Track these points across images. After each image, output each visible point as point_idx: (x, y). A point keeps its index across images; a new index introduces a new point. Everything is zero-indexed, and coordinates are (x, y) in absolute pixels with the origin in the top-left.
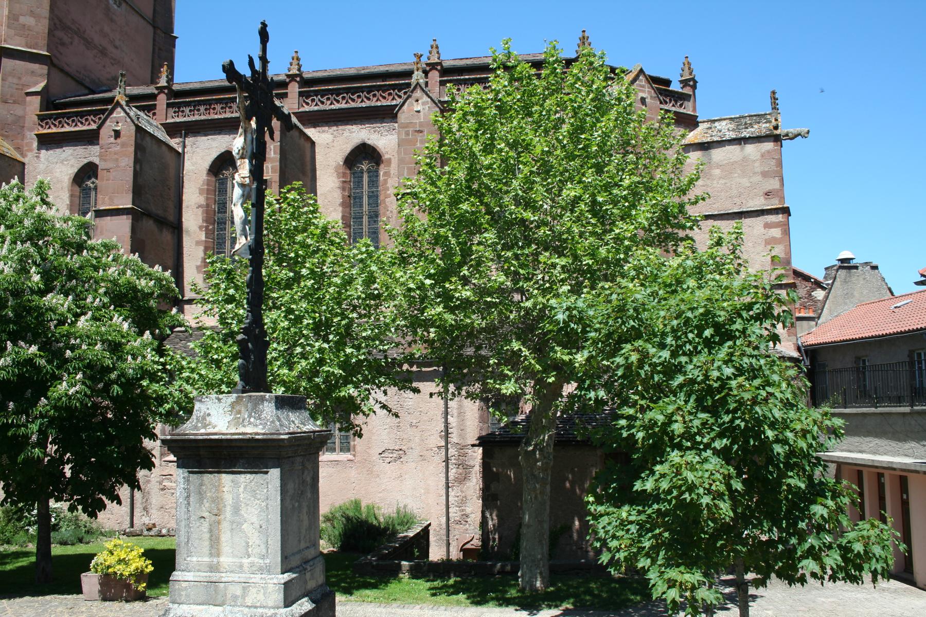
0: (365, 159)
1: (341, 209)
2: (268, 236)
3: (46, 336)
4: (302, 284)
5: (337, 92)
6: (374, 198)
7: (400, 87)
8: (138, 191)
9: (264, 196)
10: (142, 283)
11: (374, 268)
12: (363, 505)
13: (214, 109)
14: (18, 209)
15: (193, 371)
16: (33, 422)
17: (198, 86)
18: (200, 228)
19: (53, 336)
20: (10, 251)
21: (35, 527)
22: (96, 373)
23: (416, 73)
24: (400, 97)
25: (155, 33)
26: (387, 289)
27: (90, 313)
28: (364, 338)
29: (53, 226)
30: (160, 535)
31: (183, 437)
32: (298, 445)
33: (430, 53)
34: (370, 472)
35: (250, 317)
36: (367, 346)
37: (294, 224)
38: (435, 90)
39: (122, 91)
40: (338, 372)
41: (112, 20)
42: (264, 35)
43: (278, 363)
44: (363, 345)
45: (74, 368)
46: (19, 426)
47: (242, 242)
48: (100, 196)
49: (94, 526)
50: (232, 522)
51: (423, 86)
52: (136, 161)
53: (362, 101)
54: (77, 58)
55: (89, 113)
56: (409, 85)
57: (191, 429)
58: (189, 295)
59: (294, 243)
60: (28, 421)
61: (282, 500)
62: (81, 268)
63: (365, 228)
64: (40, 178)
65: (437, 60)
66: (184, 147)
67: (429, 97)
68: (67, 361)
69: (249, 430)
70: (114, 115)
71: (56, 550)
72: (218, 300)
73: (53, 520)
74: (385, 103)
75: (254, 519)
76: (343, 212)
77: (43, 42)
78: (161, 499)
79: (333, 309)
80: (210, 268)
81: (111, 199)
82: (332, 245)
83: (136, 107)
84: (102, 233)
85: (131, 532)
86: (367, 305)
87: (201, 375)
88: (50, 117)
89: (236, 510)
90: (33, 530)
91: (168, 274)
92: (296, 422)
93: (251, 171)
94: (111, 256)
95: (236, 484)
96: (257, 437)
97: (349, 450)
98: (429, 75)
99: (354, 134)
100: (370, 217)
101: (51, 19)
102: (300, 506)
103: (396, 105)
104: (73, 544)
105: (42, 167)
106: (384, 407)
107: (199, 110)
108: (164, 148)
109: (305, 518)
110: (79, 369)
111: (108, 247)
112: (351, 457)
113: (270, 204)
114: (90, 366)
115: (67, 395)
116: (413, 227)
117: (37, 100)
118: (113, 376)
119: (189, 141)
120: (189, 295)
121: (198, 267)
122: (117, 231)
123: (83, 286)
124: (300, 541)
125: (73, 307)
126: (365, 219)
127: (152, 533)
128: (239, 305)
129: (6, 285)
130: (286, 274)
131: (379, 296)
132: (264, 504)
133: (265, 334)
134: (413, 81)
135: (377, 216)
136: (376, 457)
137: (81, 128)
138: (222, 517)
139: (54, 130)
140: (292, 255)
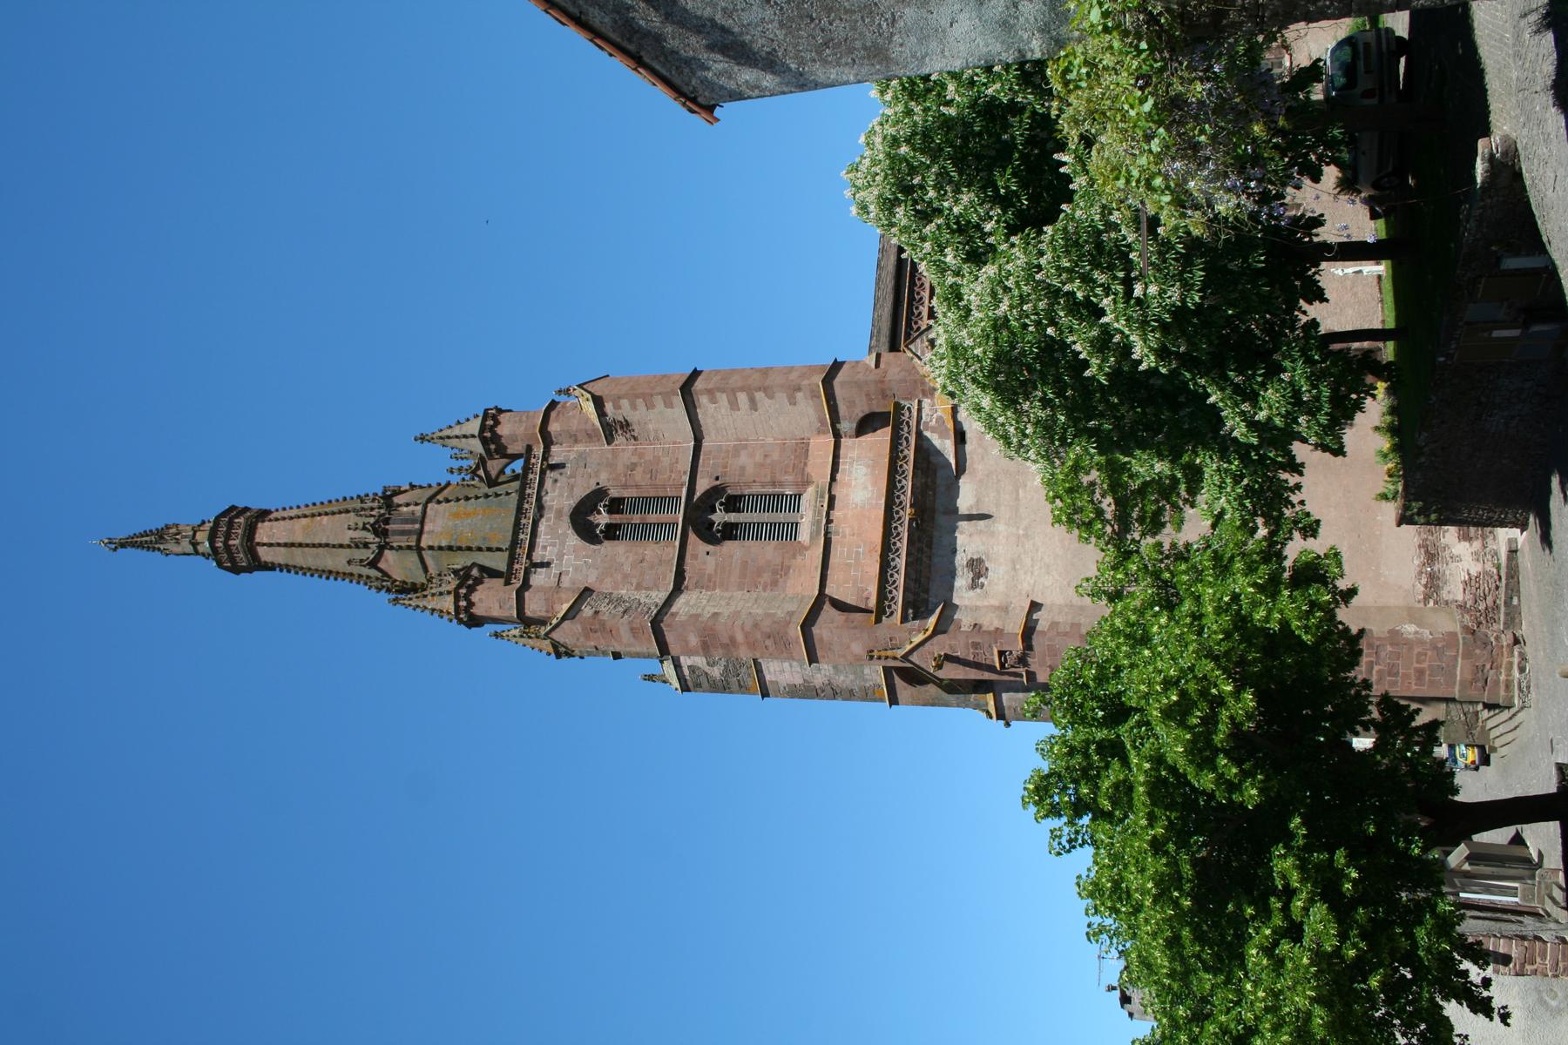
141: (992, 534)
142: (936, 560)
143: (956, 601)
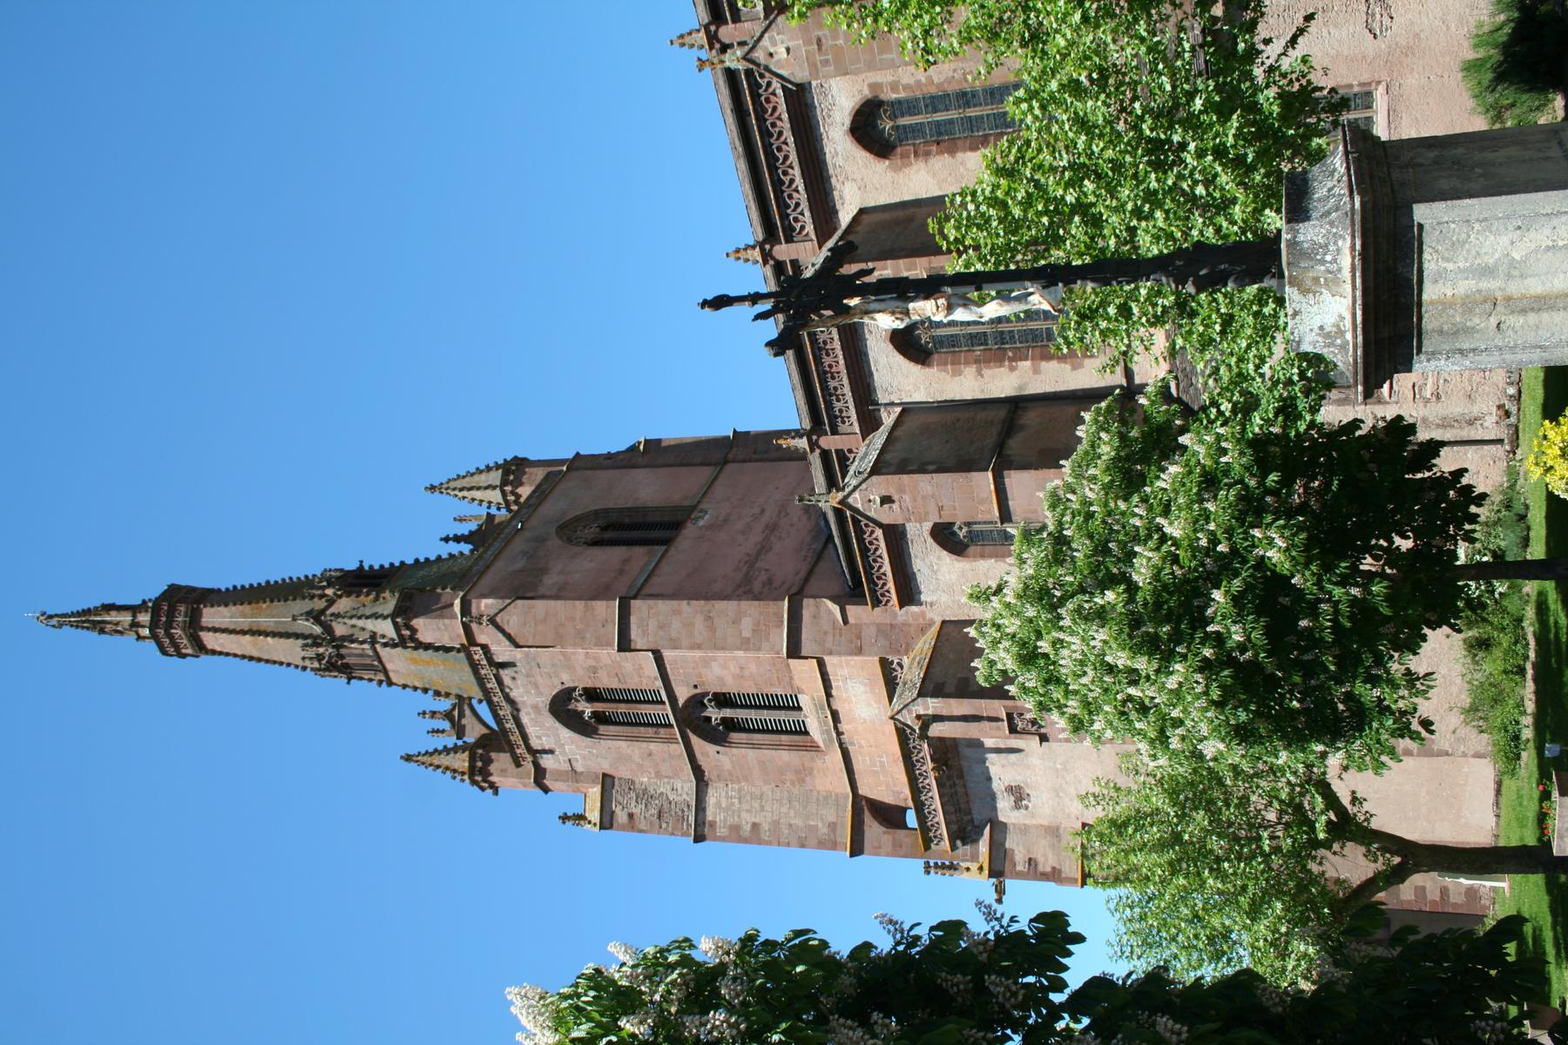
0: (875, 126)
1: (960, 155)
2: (1022, 259)
3: (1196, 579)
4: (1092, 199)
5: (778, 184)
6: (936, 102)
7: (754, 86)
8: (966, 465)
9: (958, 275)
10: (1106, 451)
11: (1054, 85)
12: (1471, 55)
13: (830, 366)
14: (1012, 625)
15: (1241, 360)
16: (1330, 593)
17: (800, 393)
18: (1012, 369)
19: (1196, 570)
20: (1073, 633)
21: (1496, 583)
22: (1250, 509)
23: (728, 64)
24: (769, 84)
25: (733, 461)
26: (1087, 58)
27: (1158, 520)
28: (1174, 87)
29: (1032, 578)
30: (1518, 397)
31: (1360, 365)
32: (1371, 176)
33: (692, 46)
34: (1409, 51)
35: (1157, 276)
36: (1187, 80)
37: (995, 224)
38: (748, 29)
39: (823, 499)
40: (1235, 121)
41: (726, 521)
42: (720, 302)
43: (1225, 224)
44: (1186, 87)
45: (1246, 539)
46: (1336, 612)
47: (1038, 301)
48: (980, 518)
49: (1497, 498)
50: (1509, 276)
51: (746, 48)
52: (922, 470)
53: (785, 143)
54: (786, 561)
55: (861, 540)
56: (749, 73)
57: (1345, 355)
58: (1119, 378)
59: (1025, 217)
60: (1329, 601)
61: (1471, 196)
62: (1090, 536)
63: (986, 110)
64: (964, 599)
65: (702, 34)
66: (892, 404)
67: (762, 36)
68: (1234, 551)
69: (1346, 261)
70: (859, 506)
71: (1537, 551)
72: (1127, 330)
73: (1485, 559)
74: (782, 107)
75: (1504, 240)
76: (964, 150)
77: (770, 607)
78: (1454, 398)
79: (1128, 143)
80: (1077, 346)
81: (982, 502)
82: (1023, 157)
83: (843, 477)
84: (1035, 511)
85: (1511, 442)
86: (1117, 89)
87: (1249, 347)
88: (873, 592)
89: (1488, 271)
90: (1501, 587)
91: (1087, 416)
92: (1330, 184)
93: (926, 298)
94: (1069, 496)
95: (1440, 276)
96: (1358, 247)
97: (1369, 94)
98: (727, 41)
99: (839, 149)
100: (967, 105)
101: (739, 598)
102: (1480, 165)
103: (784, 88)
104: (1528, 529)
105: (944, 598)
106: (1293, 41)
107: (836, 389)
108: (897, 433)
109: (1502, 154)
110: (1246, 532)
111: (1056, 501)
112: (1381, 89)
113: (967, 265)
114: (1241, 520)
115: (1287, 549)
116: (979, 28)
117: (852, 610)
118: (1253, 483)
119: (882, 398)
120: (1119, 378)
121: (1074, 368)
122: (1032, 491)
123: (1118, 532)
124: (1547, 159)
125: (1151, 544)
126: (972, 112)
127: (1514, 409)
128: (1132, 295)
129: (1124, 636)
130: (1076, 227)
131: (1102, 71)
132: (1477, 226)
133: (1180, 252)
134: (741, 66)
135: (964, 94)
136: (1381, 44)
137: (883, 550)
138: (1499, 295)
139: (891, 585)
140: (1045, 220)
141: (1028, 767)
142: (970, 785)
143: (1002, 818)
